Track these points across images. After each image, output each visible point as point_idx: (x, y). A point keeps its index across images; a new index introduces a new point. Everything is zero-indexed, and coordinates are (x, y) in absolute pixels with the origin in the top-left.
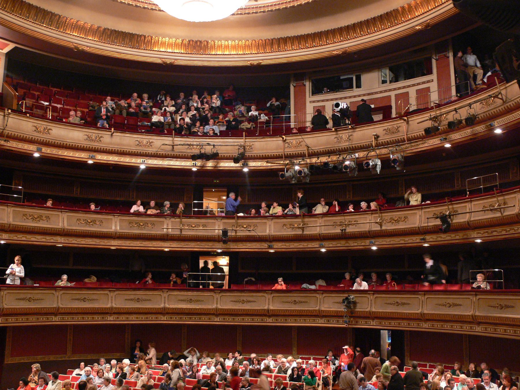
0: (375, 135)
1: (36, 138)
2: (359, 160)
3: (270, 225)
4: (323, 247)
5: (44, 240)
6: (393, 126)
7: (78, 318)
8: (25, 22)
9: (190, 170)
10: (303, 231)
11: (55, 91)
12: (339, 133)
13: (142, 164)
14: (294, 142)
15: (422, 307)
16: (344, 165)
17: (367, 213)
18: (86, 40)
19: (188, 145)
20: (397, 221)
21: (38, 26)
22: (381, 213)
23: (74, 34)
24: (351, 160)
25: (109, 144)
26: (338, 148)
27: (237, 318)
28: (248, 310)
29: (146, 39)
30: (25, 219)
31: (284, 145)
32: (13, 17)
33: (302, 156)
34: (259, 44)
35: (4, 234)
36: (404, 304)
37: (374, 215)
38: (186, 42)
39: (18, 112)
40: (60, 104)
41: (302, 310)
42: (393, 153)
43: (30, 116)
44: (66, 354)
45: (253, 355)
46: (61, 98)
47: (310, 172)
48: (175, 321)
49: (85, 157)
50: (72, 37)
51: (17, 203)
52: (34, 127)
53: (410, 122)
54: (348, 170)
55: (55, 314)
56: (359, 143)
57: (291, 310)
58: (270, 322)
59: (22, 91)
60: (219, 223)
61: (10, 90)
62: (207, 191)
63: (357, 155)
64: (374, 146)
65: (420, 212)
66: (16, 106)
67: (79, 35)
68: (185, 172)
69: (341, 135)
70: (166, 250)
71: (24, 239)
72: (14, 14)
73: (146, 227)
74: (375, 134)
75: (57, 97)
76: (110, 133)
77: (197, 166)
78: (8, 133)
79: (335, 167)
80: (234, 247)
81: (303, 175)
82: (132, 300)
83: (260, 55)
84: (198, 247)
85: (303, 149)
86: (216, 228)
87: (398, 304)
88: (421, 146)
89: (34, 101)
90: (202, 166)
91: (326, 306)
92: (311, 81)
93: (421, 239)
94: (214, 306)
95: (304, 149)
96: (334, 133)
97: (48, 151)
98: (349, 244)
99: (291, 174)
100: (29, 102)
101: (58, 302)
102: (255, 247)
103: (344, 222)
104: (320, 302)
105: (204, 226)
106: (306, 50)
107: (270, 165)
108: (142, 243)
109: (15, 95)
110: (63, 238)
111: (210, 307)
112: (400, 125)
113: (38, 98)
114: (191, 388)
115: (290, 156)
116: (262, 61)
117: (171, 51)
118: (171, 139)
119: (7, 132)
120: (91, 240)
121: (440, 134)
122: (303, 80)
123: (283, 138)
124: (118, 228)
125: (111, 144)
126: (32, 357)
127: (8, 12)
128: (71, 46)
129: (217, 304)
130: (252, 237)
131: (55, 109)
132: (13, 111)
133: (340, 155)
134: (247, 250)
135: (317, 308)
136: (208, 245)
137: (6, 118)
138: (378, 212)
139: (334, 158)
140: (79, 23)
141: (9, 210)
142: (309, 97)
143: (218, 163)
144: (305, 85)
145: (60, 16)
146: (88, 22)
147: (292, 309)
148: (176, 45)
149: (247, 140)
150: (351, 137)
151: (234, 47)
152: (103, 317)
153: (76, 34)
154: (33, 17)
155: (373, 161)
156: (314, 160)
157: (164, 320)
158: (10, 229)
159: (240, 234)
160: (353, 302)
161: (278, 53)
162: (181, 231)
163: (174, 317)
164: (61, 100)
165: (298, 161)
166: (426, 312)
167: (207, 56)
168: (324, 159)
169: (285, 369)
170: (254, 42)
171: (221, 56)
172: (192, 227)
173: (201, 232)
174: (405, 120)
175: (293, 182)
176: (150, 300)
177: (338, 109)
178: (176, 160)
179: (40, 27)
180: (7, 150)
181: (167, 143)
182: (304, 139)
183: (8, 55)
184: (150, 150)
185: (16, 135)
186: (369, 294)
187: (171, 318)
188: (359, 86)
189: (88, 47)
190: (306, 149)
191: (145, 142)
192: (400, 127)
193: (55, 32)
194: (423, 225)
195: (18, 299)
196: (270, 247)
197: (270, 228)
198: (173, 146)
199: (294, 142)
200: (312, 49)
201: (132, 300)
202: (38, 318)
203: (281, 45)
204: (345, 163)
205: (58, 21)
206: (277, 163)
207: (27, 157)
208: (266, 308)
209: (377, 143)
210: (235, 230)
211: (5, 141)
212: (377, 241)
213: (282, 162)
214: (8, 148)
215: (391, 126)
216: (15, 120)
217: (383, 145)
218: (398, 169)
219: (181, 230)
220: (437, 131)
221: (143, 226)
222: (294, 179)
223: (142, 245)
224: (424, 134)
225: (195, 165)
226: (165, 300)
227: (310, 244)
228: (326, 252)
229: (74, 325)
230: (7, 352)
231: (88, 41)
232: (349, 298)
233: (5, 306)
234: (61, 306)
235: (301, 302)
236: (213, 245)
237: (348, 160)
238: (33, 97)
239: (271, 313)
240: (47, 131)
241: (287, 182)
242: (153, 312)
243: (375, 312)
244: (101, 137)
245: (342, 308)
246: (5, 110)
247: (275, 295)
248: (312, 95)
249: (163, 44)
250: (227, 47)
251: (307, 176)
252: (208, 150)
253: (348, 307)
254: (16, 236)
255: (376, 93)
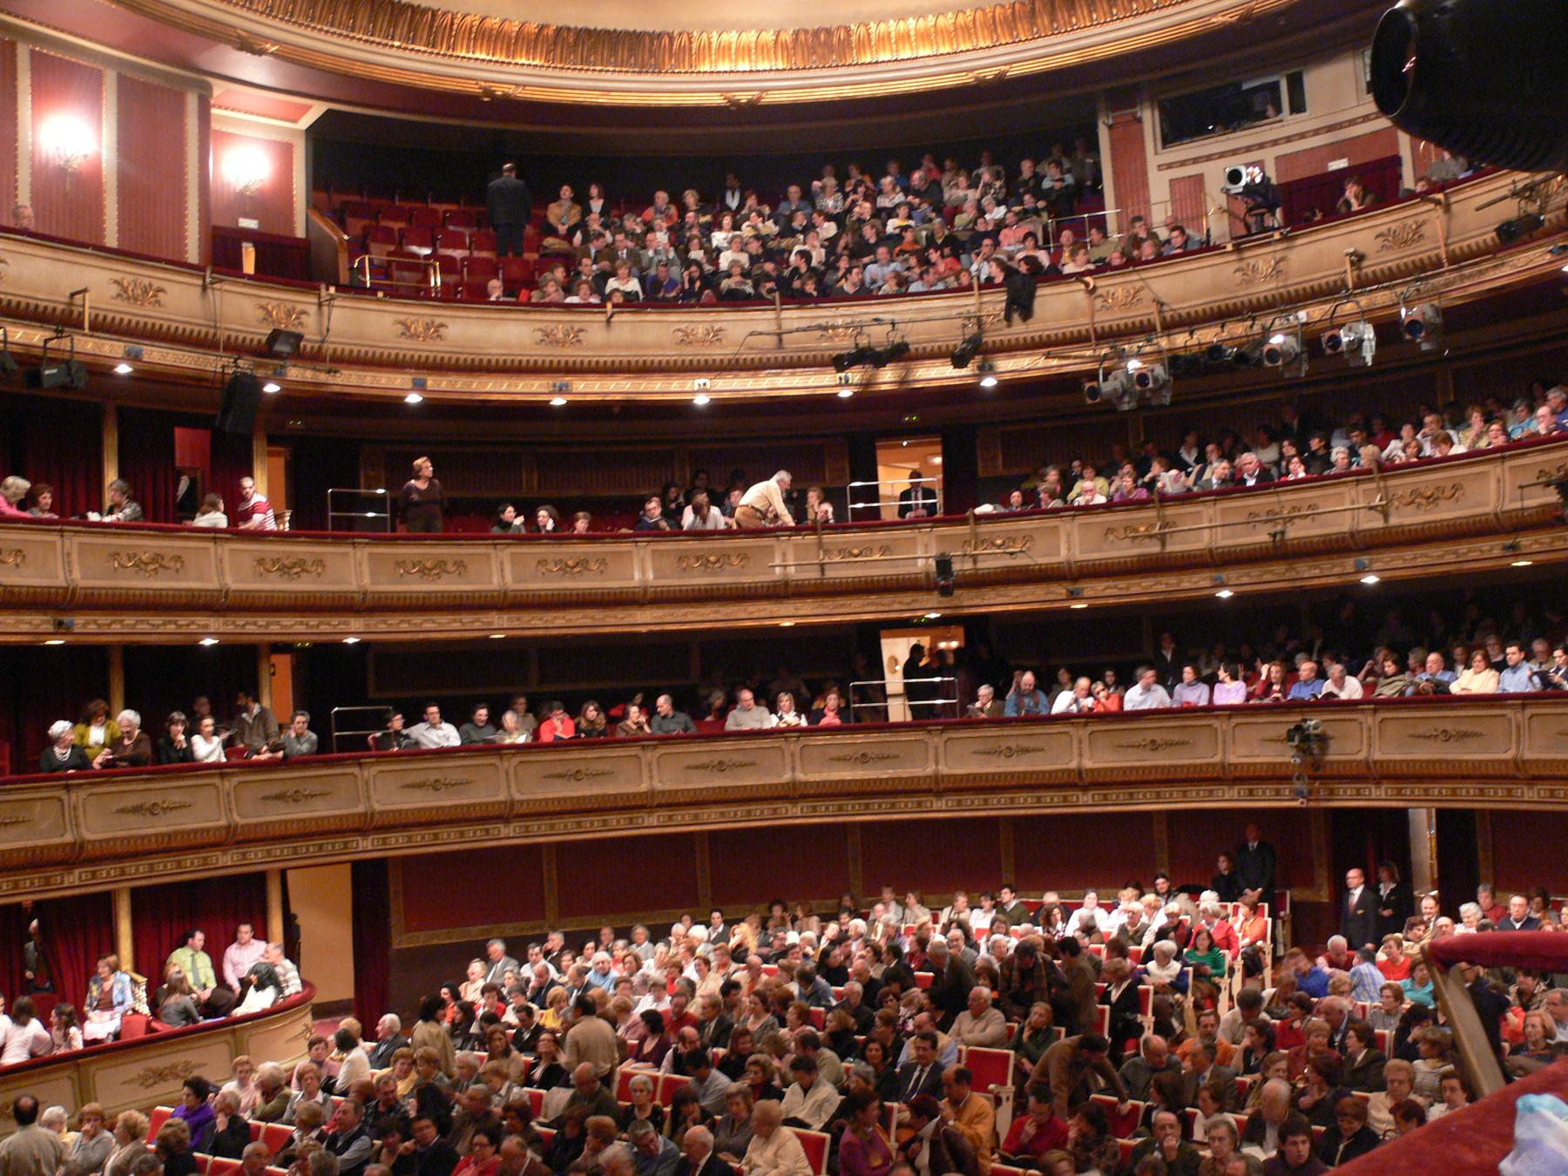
0: (1351, 254)
2: (1311, 328)
3: (1069, 535)
4: (1223, 586)
5: (456, 626)
6: (1405, 221)
7: (566, 826)
8: (347, 42)
9: (833, 398)
10: (1163, 544)
11: (445, 212)
12: (1247, 254)
13: (700, 392)
14: (1120, 292)
15: (1518, 742)
16: (1266, 348)
17: (1345, 483)
18: (511, 68)
19: (820, 327)
20: (1432, 499)
21: (380, 49)
22: (1384, 478)
23: (477, 55)
24: (1289, 331)
25: (602, 347)
26: (1246, 299)
27: (994, 799)
28: (1025, 773)
29: (676, 43)
31: (1092, 305)
32: (315, 34)
33: (1145, 330)
34: (994, 17)
36: (1464, 735)
37: (1362, 487)
38: (786, 37)
39: (354, 289)
40: (461, 246)
41: (1176, 767)
42: (1408, 302)
43: (385, 295)
44: (544, 917)
45: (1051, 898)
47: (1170, 374)
48: (825, 814)
49: (543, 390)
50: (471, 64)
51: (378, 534)
53: (1455, 208)
54: (1280, 363)
55: (504, 819)
56: (1306, 282)
57: (1144, 768)
58: (1086, 803)
59: (357, 225)
60: (926, 538)
61: (327, 228)
62: (885, 447)
63: (1303, 315)
64: (1350, 285)
65: (1499, 470)
67: (489, 58)
68: (821, 404)
69: (1252, 262)
70: (787, 623)
71: (404, 627)
72: (314, 28)
73: (727, 568)
74: (1351, 250)
75: (451, 228)
76: (603, 318)
77: (852, 385)
79: (1241, 358)
80: (972, 603)
81: (1151, 385)
82: (704, 767)
83: (1001, 50)
84: (873, 608)
85: (1145, 311)
86: (919, 554)
87: (1447, 736)
88: (1491, 275)
89: (392, 248)
90: (867, 384)
91: (1241, 751)
92: (1156, 104)
93: (1506, 548)
94: (929, 770)
95: (1150, 311)
96: (1234, 257)
98: (1298, 572)
99: (1117, 384)
100: (379, 253)
101: (509, 787)
102: (1029, 598)
103: (1277, 510)
104: (1224, 741)
105: (885, 549)
106: (1131, 21)
107: (1055, 362)
108: (717, 612)
109: (341, 240)
110: (505, 617)
111: (918, 772)
112: (1424, 217)
113: (402, 239)
114: (929, 977)
115: (1104, 336)
116: (1007, 68)
117: (748, 69)
118: (771, 315)
119: (332, 347)
120: (580, 615)
121: (1548, 234)
122: (1133, 106)
123: (1087, 284)
124: (650, 576)
125: (609, 346)
127: (301, 25)
128: (474, 89)
129: (937, 763)
130: (1021, 572)
131: (448, 266)
132: (341, 289)
133: (1254, 319)
134: (1011, 608)
135: (1217, 759)
136: (901, 603)
137: (325, 309)
138: (1376, 475)
139: (1238, 329)
140: (489, 23)
141: (359, 553)
142: (1156, 153)
143: (908, 371)
144: (1140, 121)
145: (434, 13)
146: (509, 17)
147: (1147, 763)
148: (761, 49)
149: (985, 299)
150: (1281, 264)
151: (925, 36)
152: (631, 819)
153: (483, 56)
154: (364, 24)
155: (1350, 330)
156: (1181, 339)
157: (795, 815)
159: (987, 564)
160: (1317, 735)
161: (1053, 39)
162: (823, 571)
163: (822, 805)
164: (462, 236)
165: (1135, 347)
166: (1528, 755)
167: (852, 70)
168: (1208, 335)
169: (1136, 932)
170: (979, 14)
171: (890, 66)
172: (851, 554)
173: (877, 567)
174: (1438, 202)
175: (1126, 407)
176: (752, 764)
177: (1238, 188)
178: (793, 374)
179: (387, 50)
180: (338, 394)
181: (761, 327)
182: (1150, 282)
183: (313, 132)
184: (718, 353)
185: (355, 353)
186: (1363, 710)
187: (814, 808)
188: (1298, 106)
189: (517, 85)
190: (1154, 308)
191: (700, 331)
192: (1424, 223)
193: (426, 57)
194: (1508, 506)
195: (408, 786)
196: (1073, 595)
197: (1068, 541)
198: (779, 335)
199: (1120, 292)
200: (1151, 16)
201: (704, 767)
202: (462, 833)
203: (1060, 15)
204: (1272, 341)
205: (431, 26)
206: (1075, 357)
208: (1073, 765)
209: (1359, 277)
210: (972, 556)
211: (329, 372)
212: (1377, 561)
213: (1089, 353)
214: (337, 389)
215: (1398, 223)
216: (348, 313)
217: (1376, 280)
218: (1425, 347)
219: (822, 566)
220: (1537, 228)
221: (718, 565)
222: (1126, 399)
223: (719, 617)
224: (1497, 240)
225: (847, 381)
226: (793, 762)
227: (1185, 578)
228: (1231, 598)
229: (558, 844)
230: (396, 919)
231: (518, 69)
232: (1305, 726)
234: (518, 797)
235: (1171, 744)
236: (913, 601)
237: (1276, 332)
238: (387, 236)
239: (1088, 780)
240: (435, 330)
241: (1109, 406)
242: (764, 794)
243: (1382, 762)
244: (581, 330)
245: (1287, 756)
247: (1095, 728)
248: (1164, 148)
249: (724, 50)
250: (904, 38)
251: (1162, 387)
252: (878, 336)
253: (1303, 750)
254: (385, 622)
255: (1352, 122)
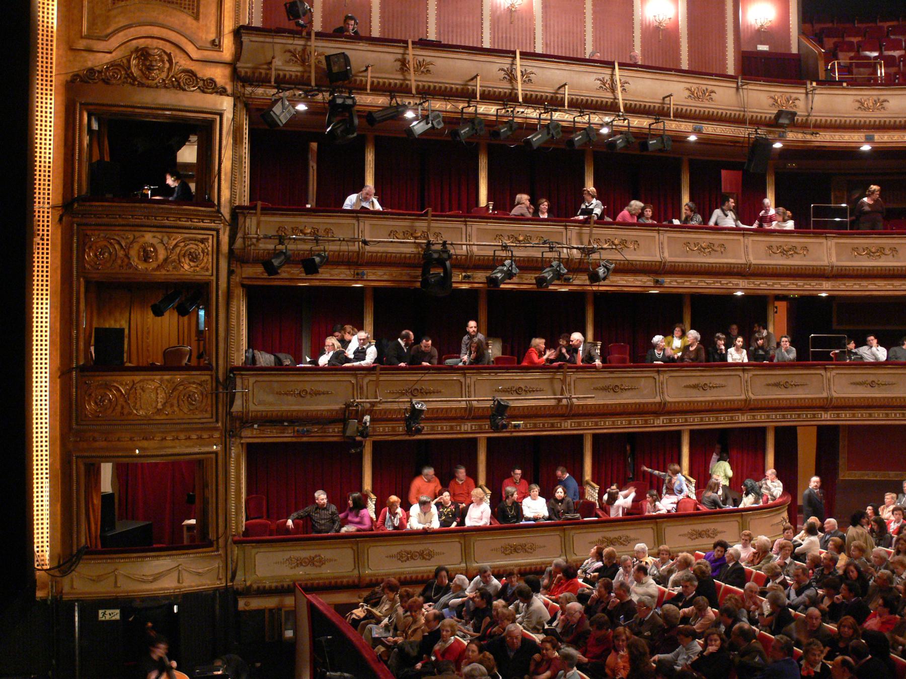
1: (863, 120)
30: (855, 256)
35: (824, 283)
39: (829, 82)
43: (847, 85)
46: (900, 37)
51: (840, 230)
52: (771, 100)
66: (824, 73)
71: (856, 287)
75: (892, 37)
78: (816, 120)
89: (852, 54)
97: (885, 138)
100: (844, 58)
109: (820, 53)
119: (814, 119)
126: (881, 473)
132: (820, 83)
137: (810, 96)
141: (829, 243)
158: (833, 273)
207: (851, 153)
211: (812, 134)
230: (842, 461)
233: (835, 395)
238: (850, 47)
246: (806, 84)
